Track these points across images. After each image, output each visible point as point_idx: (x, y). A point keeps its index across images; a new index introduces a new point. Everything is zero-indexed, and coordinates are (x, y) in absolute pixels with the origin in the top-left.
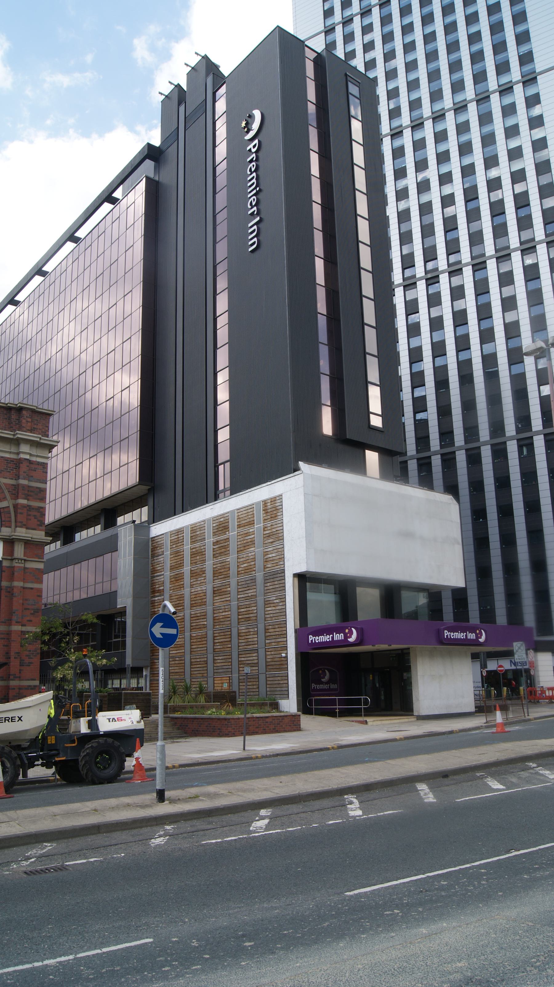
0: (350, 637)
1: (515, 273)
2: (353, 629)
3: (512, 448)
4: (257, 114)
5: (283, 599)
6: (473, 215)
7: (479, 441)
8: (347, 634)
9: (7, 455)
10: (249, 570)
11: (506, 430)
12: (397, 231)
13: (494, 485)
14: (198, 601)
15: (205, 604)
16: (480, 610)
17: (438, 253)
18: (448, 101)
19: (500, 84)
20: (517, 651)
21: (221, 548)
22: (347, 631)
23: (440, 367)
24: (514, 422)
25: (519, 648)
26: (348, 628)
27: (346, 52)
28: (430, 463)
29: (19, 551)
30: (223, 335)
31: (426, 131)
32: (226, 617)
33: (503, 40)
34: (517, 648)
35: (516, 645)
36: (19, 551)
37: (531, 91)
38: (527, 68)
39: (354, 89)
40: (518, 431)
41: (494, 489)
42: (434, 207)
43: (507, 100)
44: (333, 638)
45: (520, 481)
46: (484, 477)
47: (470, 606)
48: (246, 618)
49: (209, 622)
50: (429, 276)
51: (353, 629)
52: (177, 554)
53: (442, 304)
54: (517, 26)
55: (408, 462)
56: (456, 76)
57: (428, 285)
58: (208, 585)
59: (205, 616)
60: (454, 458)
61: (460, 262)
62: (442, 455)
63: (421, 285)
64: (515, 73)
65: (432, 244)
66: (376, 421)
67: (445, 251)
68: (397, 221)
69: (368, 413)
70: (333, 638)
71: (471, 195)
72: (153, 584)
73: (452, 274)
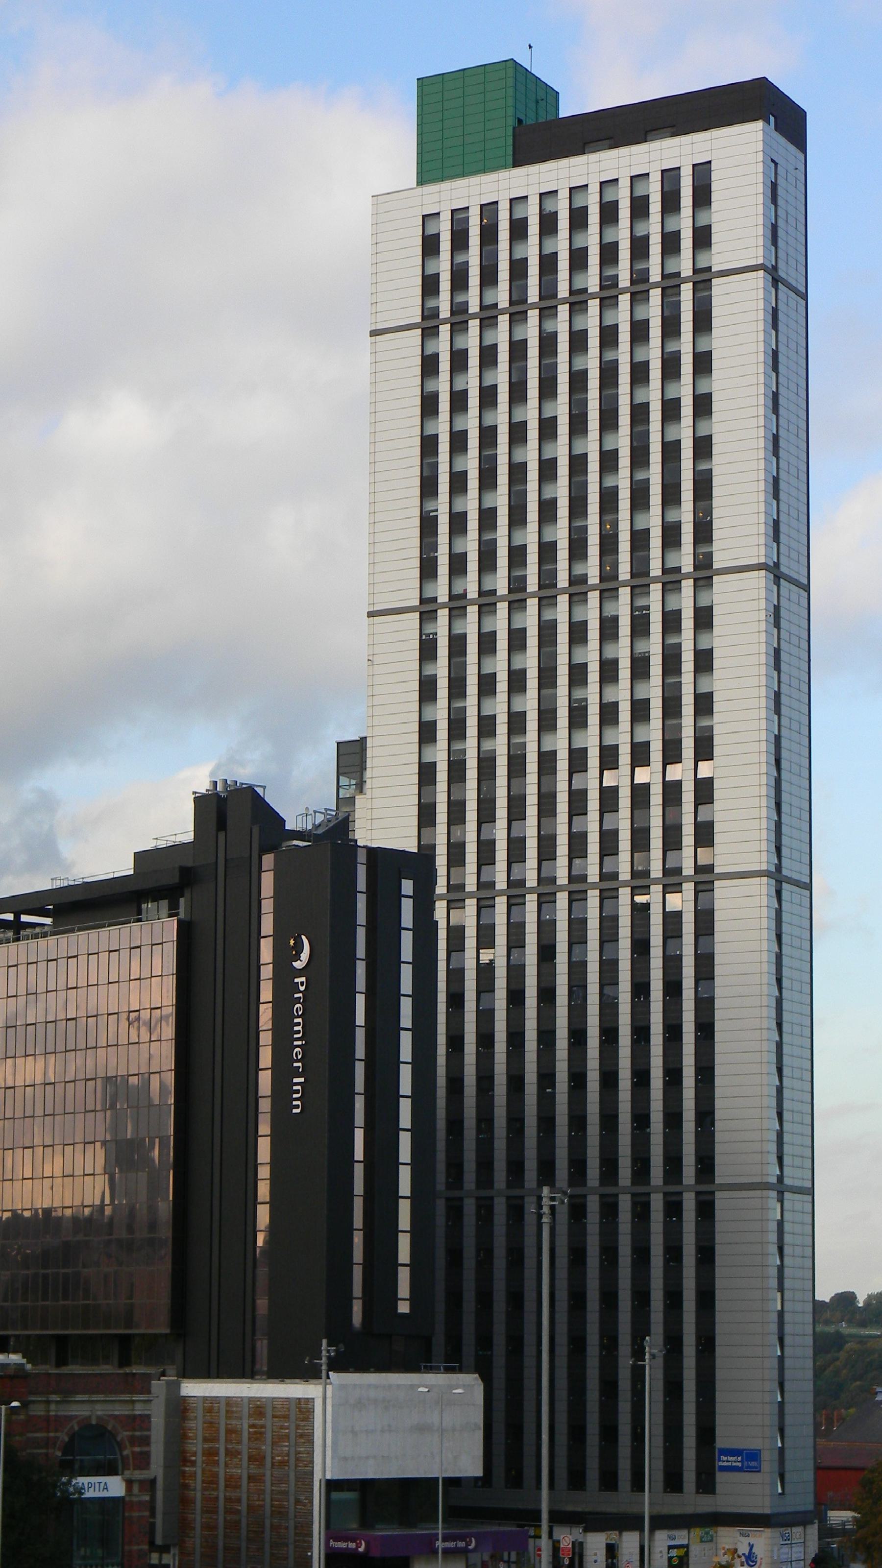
0: (297, 958)
4: (363, 1542)
5: (311, 1502)
9: (127, 1413)
10: (283, 1463)
14: (232, 1483)
15: (239, 1487)
21: (257, 1435)
29: (136, 1489)
30: (264, 1190)
32: (260, 1506)
36: (136, 1489)
39: (407, 887)
48: (280, 1512)
49: (243, 1508)
51: (303, 937)
52: (211, 1425)
54: (639, 721)
58: (242, 1470)
59: (239, 1500)
66: (404, 1308)
69: (395, 1299)
72: (184, 1452)
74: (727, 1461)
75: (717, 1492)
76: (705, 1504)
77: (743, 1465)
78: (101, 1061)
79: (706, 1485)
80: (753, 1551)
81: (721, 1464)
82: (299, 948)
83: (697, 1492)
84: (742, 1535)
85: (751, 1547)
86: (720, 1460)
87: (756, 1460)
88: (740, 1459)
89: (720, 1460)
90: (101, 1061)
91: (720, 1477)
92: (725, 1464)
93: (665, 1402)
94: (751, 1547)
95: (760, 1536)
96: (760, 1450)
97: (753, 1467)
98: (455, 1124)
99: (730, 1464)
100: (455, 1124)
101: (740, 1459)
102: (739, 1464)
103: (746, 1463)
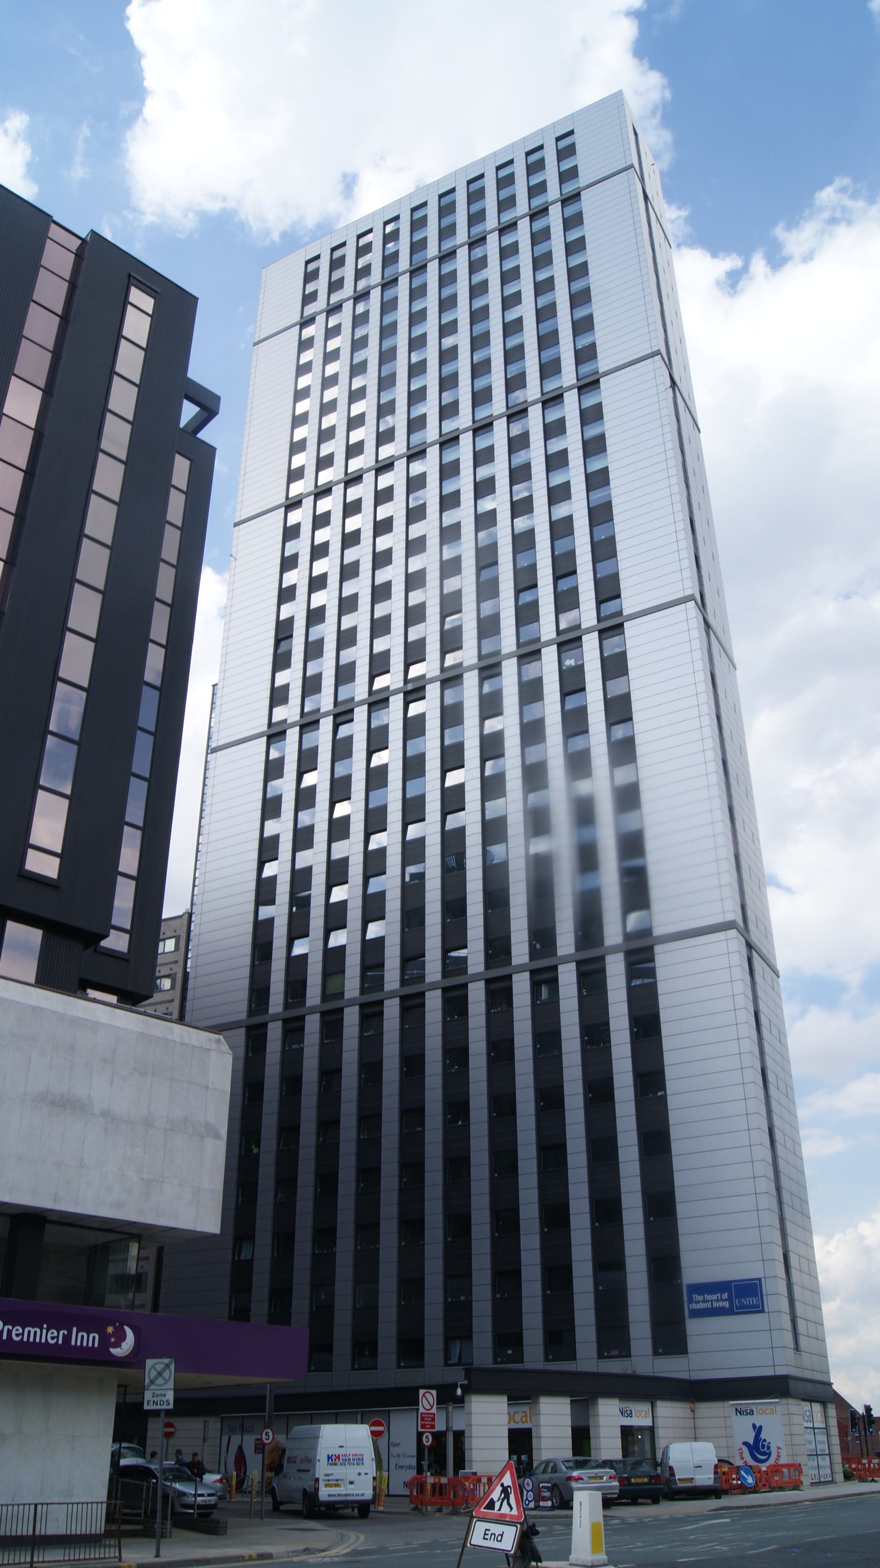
0: (118, 1345)
1: (587, 668)
2: (126, 1328)
3: (568, 976)
6: (487, 589)
7: (467, 973)
8: (110, 1336)
11: (558, 944)
12: (588, 539)
13: (628, 1031)
16: (597, 1292)
17: (622, 587)
18: (533, 390)
19: (545, 391)
20: (152, 1382)
22: (110, 1329)
23: (493, 821)
24: (527, 939)
25: (160, 1374)
26: (113, 1325)
27: (413, 311)
28: (465, 998)
31: (602, 393)
33: (555, 328)
34: (153, 1374)
35: (153, 1367)
37: (590, 401)
38: (586, 369)
40: (533, 954)
41: (628, 1039)
42: (538, 538)
43: (553, 415)
44: (67, 1338)
45: (628, 1032)
46: (661, 1006)
47: (576, 1283)
50: (410, 687)
51: (126, 1328)
53: (630, 672)
55: (427, 994)
56: (548, 354)
57: (482, 680)
60: (603, 970)
61: (498, 653)
62: (579, 963)
63: (550, 655)
64: (568, 376)
65: (612, 571)
67: (593, 596)
68: (549, 536)
70: (67, 1338)
71: (487, 558)
73: (604, 633)
74: (705, 1301)
75: (689, 1350)
76: (671, 1367)
77: (731, 1304)
78: (12, 1557)
79: (670, 1337)
80: (763, 1436)
81: (694, 1306)
82: (123, 1337)
83: (656, 1353)
84: (739, 1412)
85: (758, 1430)
86: (691, 1300)
87: (756, 1295)
88: (725, 1296)
89: (691, 1300)
90: (12, 1557)
91: (694, 1327)
92: (702, 1306)
93: (545, 1296)
94: (758, 1430)
95: (773, 1412)
96: (760, 1280)
97: (750, 1307)
98: (292, 1082)
99: (709, 1305)
100: (292, 1082)
101: (725, 1296)
102: (726, 1305)
103: (736, 1302)
